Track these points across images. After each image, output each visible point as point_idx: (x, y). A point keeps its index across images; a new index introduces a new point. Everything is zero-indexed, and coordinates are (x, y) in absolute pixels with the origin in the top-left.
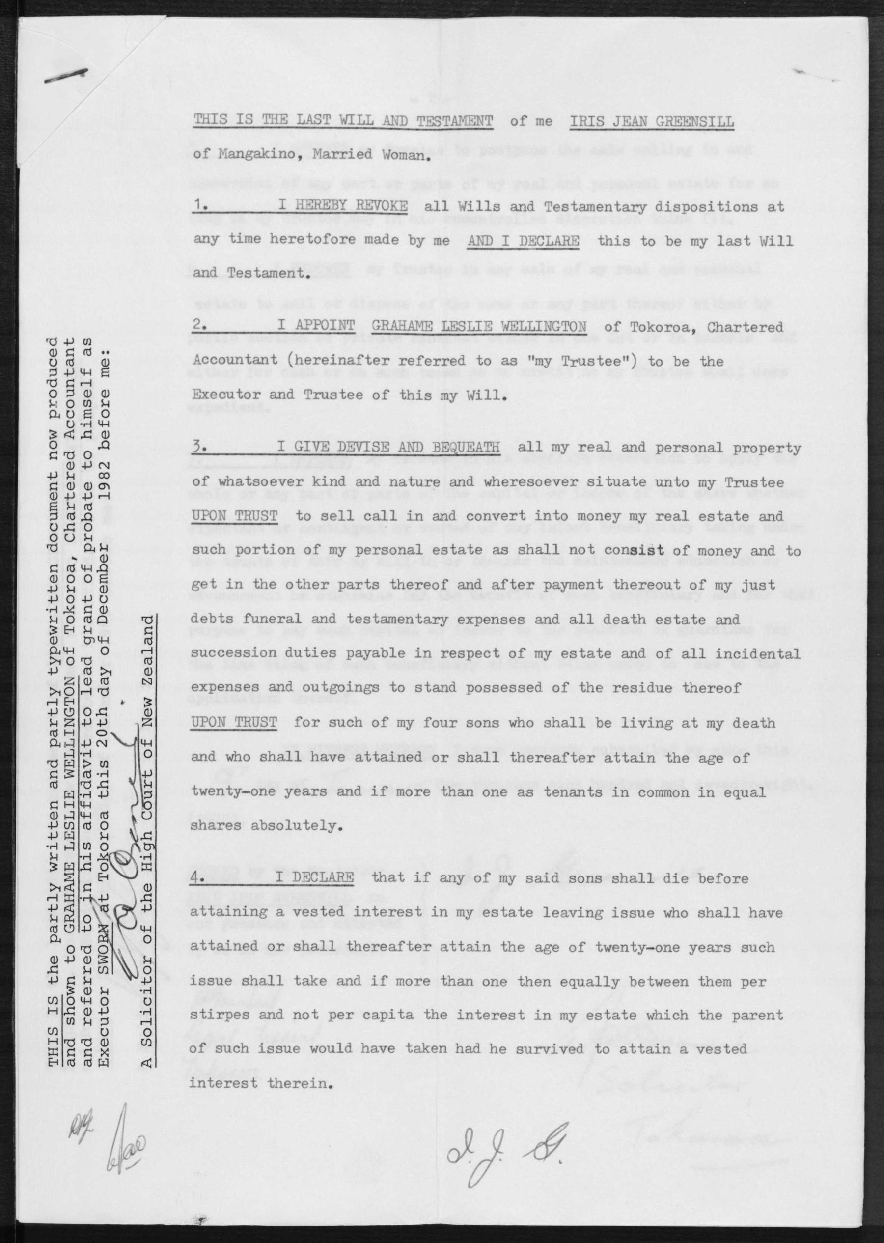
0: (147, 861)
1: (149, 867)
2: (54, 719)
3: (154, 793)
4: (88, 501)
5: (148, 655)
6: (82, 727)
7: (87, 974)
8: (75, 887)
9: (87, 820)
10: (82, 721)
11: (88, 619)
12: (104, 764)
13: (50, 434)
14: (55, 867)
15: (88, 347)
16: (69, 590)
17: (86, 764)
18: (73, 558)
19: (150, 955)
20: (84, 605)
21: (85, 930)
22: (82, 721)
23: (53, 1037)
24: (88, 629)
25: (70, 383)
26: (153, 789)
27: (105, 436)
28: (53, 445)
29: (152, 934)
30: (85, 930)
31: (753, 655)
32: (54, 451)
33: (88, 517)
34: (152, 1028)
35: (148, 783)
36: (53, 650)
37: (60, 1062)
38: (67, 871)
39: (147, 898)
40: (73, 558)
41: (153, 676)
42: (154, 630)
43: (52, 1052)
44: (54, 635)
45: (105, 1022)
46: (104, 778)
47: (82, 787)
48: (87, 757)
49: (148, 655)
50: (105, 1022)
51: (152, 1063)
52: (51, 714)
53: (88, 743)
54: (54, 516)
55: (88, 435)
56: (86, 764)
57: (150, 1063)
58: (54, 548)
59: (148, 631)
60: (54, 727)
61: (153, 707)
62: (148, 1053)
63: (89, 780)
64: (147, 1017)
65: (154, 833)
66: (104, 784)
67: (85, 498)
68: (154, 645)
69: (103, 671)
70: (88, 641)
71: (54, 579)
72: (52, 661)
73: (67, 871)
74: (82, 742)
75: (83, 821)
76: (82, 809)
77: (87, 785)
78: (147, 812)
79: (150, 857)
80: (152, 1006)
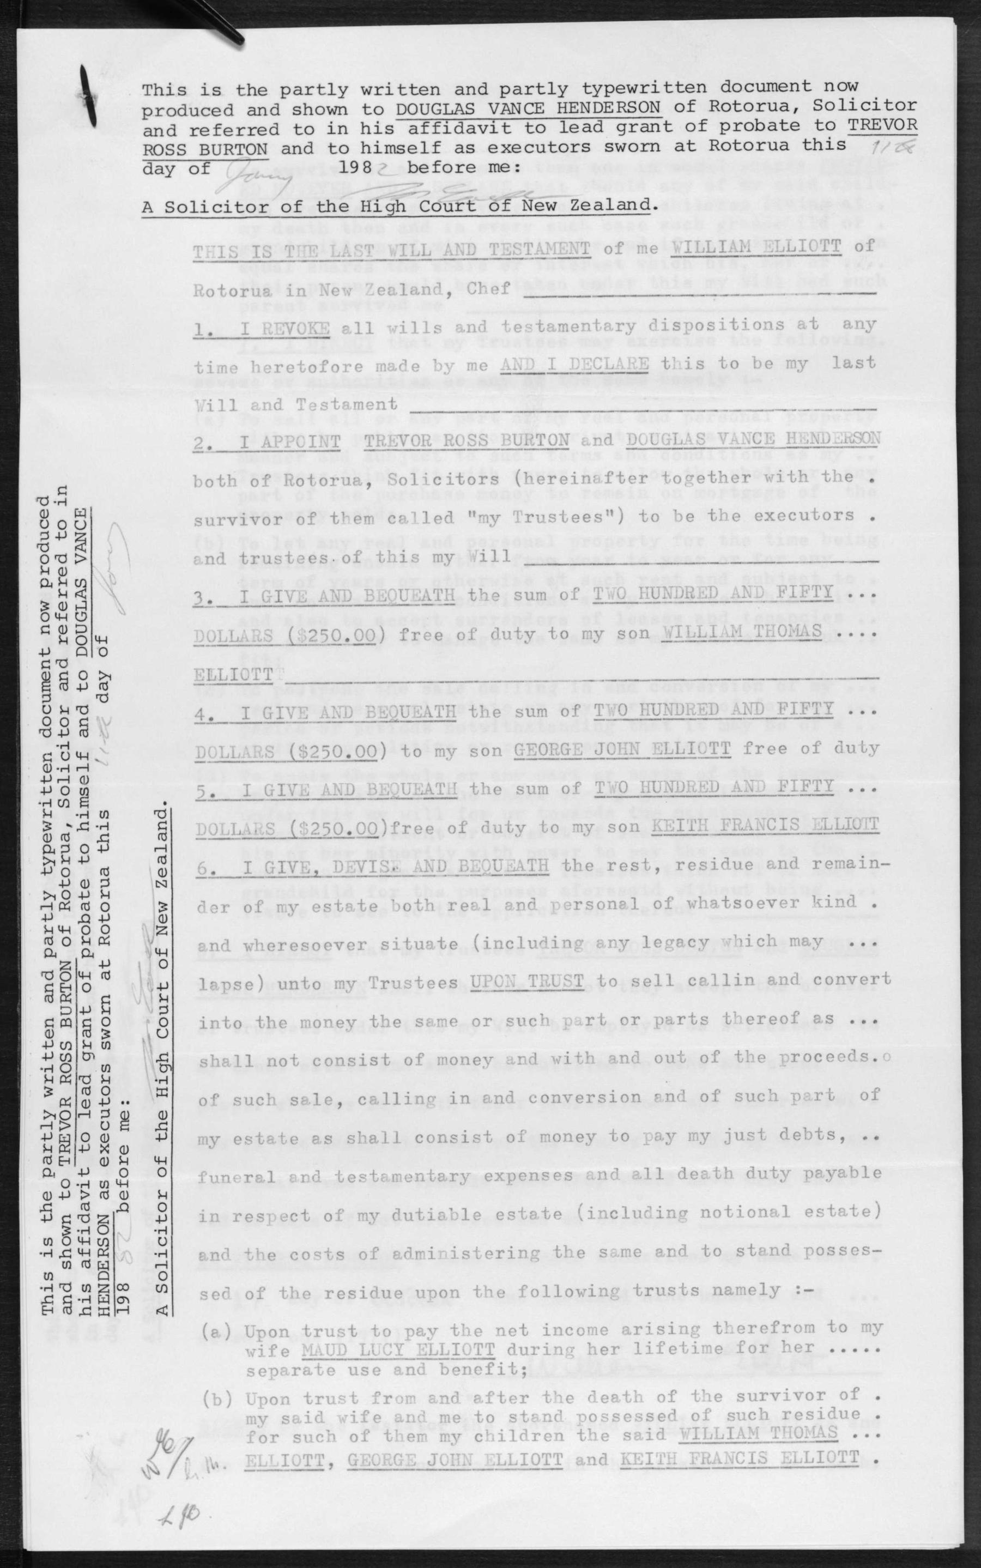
0: (163, 1085)
1: (366, 209)
2: (534, 91)
3: (450, 214)
7: (248, 131)
8: (506, 115)
9: (420, 130)
10: (531, 122)
12: (586, 148)
14: (366, 92)
16: (158, 110)
17: (483, 128)
18: (796, 109)
19: (165, 1189)
21: (528, 126)
30: (528, 126)
31: (85, 1219)
32: (476, 92)
33: (760, 127)
35: (461, 207)
36: (610, 89)
39: (331, 207)
40: (796, 109)
41: (168, 878)
42: (168, 826)
44: (627, 90)
45: (105, 1114)
47: (456, 123)
48: (490, 129)
49: (162, 853)
50: (541, 149)
51: (169, 1311)
52: (319, 87)
53: (508, 130)
54: (761, 88)
55: (84, 826)
56: (483, 128)
59: (162, 826)
60: (524, 90)
61: (168, 913)
62: (159, 209)
63: (465, 131)
64: (199, 208)
65: (404, 214)
68: (168, 842)
70: (86, 1057)
71: (422, 91)
72: (597, 87)
74: (80, 1009)
76: (432, 123)
77: (459, 130)
79: (377, 211)
80: (211, 214)
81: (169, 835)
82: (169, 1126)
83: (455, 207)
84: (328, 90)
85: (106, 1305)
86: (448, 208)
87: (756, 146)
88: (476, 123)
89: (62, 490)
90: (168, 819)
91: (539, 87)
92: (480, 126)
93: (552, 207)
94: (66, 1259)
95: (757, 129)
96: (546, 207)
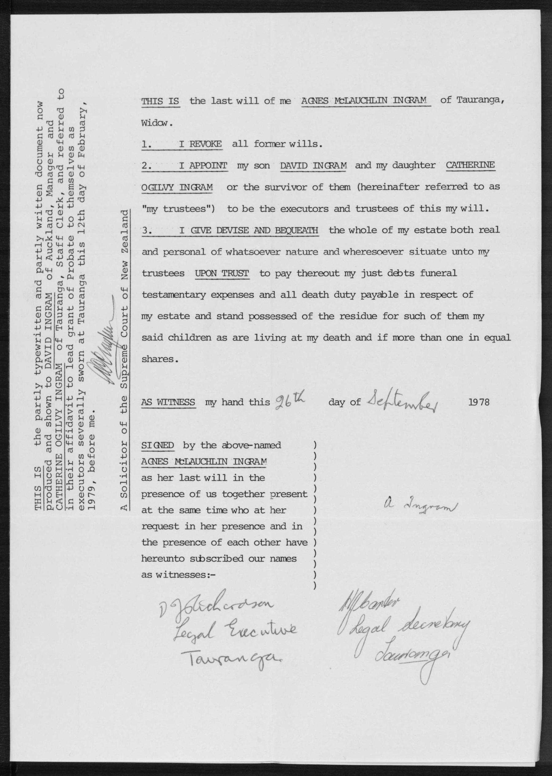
2: (38, 402)
3: (128, 320)
4: (71, 248)
5: (125, 234)
6: (67, 388)
7: (61, 126)
9: (70, 446)
10: (67, 385)
11: (71, 321)
12: (82, 244)
13: (38, 104)
14: (40, 226)
15: (72, 133)
17: (69, 411)
19: (126, 440)
20: (68, 312)
21: (69, 386)
22: (67, 385)
23: (38, 492)
24: (71, 327)
25: (71, 315)
26: (128, 318)
27: (92, 464)
28: (40, 111)
29: (127, 428)
30: (69, 386)
33: (71, 257)
34: (128, 486)
36: (38, 360)
37: (42, 507)
38: (58, 485)
43: (37, 502)
44: (38, 350)
45: (82, 482)
46: (82, 254)
47: (67, 426)
48: (70, 407)
49: (125, 234)
50: (82, 482)
51: (128, 508)
53: (70, 398)
54: (40, 155)
56: (69, 411)
57: (126, 508)
58: (40, 174)
59: (125, 219)
61: (128, 267)
64: (124, 479)
66: (82, 258)
67: (69, 245)
69: (81, 187)
70: (71, 334)
72: (37, 366)
73: (58, 485)
74: (67, 398)
75: (67, 447)
76: (66, 439)
77: (70, 424)
78: (125, 332)
81: (129, 225)
82: (128, 405)
83: (125, 318)
84: (38, 395)
85: (60, 485)
86: (125, 321)
87: (92, 446)
88: (67, 416)
89: (300, 527)
90: (128, 215)
91: (37, 252)
92: (68, 413)
93: (126, 264)
94: (48, 421)
95: (73, 259)
96: (125, 267)
